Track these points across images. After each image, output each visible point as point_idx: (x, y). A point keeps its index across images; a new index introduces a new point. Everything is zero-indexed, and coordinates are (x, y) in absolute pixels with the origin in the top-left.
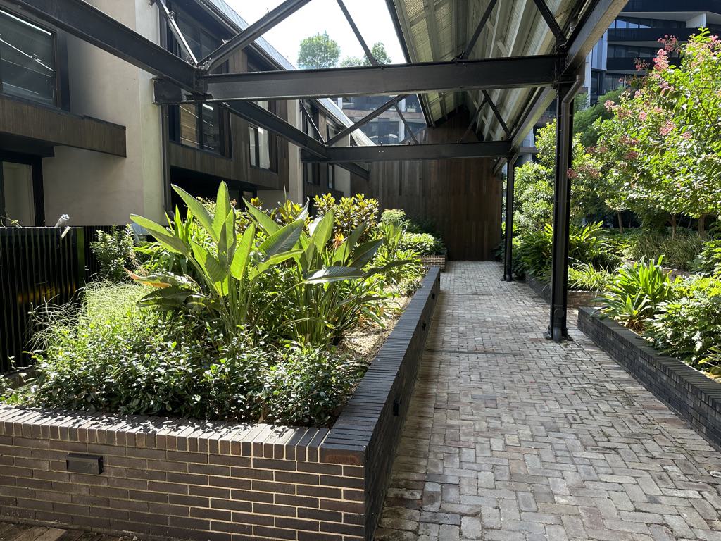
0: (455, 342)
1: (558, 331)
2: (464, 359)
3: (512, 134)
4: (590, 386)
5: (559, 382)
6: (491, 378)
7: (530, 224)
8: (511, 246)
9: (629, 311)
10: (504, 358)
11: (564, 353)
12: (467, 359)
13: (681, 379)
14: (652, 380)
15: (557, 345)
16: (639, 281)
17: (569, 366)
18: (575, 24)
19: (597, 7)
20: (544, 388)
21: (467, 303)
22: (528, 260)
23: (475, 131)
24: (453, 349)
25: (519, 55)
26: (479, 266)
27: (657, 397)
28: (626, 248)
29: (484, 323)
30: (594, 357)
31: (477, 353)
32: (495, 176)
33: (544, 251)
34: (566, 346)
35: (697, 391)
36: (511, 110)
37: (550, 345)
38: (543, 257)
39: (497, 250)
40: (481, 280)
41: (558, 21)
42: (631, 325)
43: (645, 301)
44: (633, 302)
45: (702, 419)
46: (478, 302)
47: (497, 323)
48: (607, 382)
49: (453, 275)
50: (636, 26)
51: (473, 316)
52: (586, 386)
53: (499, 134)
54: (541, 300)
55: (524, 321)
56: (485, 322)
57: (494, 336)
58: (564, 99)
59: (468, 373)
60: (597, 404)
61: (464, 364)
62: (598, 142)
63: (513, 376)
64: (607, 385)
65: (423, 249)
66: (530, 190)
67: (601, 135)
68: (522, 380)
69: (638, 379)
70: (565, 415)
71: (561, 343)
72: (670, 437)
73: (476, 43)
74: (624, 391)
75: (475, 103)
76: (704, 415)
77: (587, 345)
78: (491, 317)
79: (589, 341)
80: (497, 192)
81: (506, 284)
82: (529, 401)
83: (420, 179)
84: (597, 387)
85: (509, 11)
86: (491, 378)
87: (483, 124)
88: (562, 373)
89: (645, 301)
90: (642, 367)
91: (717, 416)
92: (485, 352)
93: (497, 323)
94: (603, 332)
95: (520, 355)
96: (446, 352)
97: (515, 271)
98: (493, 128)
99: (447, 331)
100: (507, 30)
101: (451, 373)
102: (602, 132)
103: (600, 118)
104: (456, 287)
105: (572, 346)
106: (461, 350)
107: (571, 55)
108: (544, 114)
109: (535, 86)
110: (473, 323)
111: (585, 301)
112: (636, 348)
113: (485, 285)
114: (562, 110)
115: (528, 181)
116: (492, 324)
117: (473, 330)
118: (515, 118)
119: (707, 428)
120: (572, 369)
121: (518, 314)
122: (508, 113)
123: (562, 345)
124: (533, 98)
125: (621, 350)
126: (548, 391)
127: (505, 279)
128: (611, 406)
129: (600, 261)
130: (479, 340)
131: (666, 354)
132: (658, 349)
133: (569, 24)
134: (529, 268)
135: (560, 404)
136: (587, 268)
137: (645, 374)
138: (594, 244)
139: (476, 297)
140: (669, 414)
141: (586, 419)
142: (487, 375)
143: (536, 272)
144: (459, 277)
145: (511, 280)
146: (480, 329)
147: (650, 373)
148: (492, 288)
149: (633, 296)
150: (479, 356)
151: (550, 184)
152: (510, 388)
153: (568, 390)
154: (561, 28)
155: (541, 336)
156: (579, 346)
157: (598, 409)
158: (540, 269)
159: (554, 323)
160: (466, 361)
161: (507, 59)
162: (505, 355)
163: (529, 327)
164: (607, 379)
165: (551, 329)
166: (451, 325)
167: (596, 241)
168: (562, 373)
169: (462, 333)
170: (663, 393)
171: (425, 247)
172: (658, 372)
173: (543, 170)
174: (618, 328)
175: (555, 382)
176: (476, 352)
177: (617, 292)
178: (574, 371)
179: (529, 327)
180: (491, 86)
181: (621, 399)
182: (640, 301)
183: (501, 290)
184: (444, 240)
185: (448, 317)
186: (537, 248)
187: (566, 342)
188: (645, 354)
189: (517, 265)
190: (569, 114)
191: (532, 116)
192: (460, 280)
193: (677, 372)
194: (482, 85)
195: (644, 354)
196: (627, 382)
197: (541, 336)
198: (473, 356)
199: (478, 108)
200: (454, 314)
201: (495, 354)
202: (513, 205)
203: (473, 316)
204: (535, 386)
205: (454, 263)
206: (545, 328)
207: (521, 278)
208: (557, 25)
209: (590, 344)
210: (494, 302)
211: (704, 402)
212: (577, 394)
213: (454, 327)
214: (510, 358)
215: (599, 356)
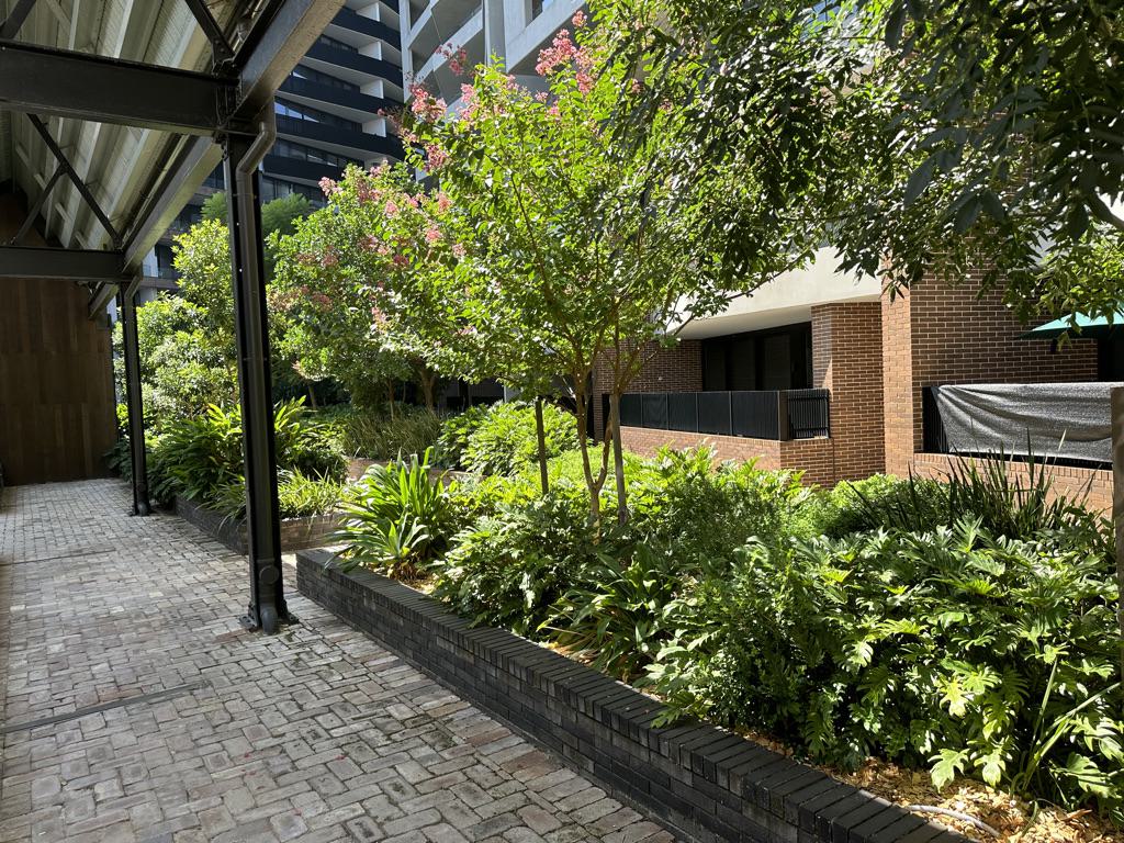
0: (41, 692)
1: (269, 610)
2: (69, 739)
3: (125, 240)
4: (365, 723)
5: (304, 732)
6: (148, 777)
7: (173, 405)
8: (144, 449)
9: (392, 550)
10: (170, 705)
11: (289, 655)
12: (78, 736)
13: (531, 673)
14: (469, 679)
15: (271, 639)
16: (400, 494)
17: (310, 684)
18: (246, 28)
19: (252, 58)
20: (278, 763)
21: (61, 580)
22: (182, 473)
23: (42, 234)
24: (37, 716)
25: (138, 59)
26: (78, 489)
27: (483, 711)
28: (331, 437)
29: (107, 624)
30: (348, 649)
31: (101, 710)
32: (93, 319)
33: (211, 454)
34: (289, 638)
35: (566, 694)
36: (120, 191)
37: (260, 643)
38: (211, 464)
39: (111, 456)
40: (87, 520)
41: (114, 224)
42: (397, 575)
43: (415, 529)
44: (398, 531)
45: (583, 746)
46: (87, 571)
47: (138, 616)
48: (389, 701)
49: (19, 517)
50: (299, 116)
51: (79, 608)
52: (356, 726)
53: (97, 238)
54: (215, 545)
55: (194, 598)
56: (112, 618)
57: (136, 652)
58: (240, 165)
59: (87, 781)
60: (393, 767)
61: (74, 754)
62: (276, 270)
63: (201, 752)
64: (391, 709)
66: (168, 346)
67: (278, 259)
68: (224, 754)
69: (439, 678)
70: (344, 825)
71: (279, 632)
72: (545, 805)
73: (32, 12)
74: (425, 715)
75: (38, 177)
76: (589, 739)
77: (326, 624)
78: (121, 604)
79: (328, 616)
80: (101, 350)
81: (141, 521)
82: (255, 815)
84: (379, 721)
85: (96, 25)
86: (148, 777)
87: (59, 220)
88: (300, 707)
89: (415, 529)
90: (446, 655)
91: (615, 740)
92: (121, 702)
93: (136, 616)
94: (354, 596)
95: (207, 684)
96: (17, 729)
97: (156, 493)
98: (82, 228)
99: (15, 666)
100: (103, 21)
101: (37, 797)
102: (280, 254)
103: (277, 231)
104: (30, 544)
105: (302, 635)
106: (59, 711)
107: (247, 84)
108: (171, 226)
109: (178, 129)
110: (81, 627)
111: (296, 535)
112: (429, 621)
113: (98, 530)
114: (238, 184)
115: (159, 332)
116: (125, 622)
117: (83, 648)
118: (129, 211)
119: (596, 762)
120: (317, 690)
121: (180, 585)
122: (112, 202)
123: (281, 636)
124: (163, 174)
125: (396, 627)
126: (288, 767)
127: (136, 512)
128: (419, 761)
129: (309, 463)
130: (103, 669)
131: (484, 623)
132: (464, 616)
133: (235, 25)
134: (182, 488)
135: (324, 798)
136: (291, 476)
137: (452, 668)
138: (298, 435)
139: (80, 560)
140: (517, 746)
141: (388, 819)
142: (136, 772)
143: (200, 494)
145: (149, 512)
146: (100, 640)
147: (463, 665)
148: (112, 535)
149: (397, 522)
150: (110, 715)
151: (206, 333)
152: (203, 791)
153: (327, 751)
154: (222, 27)
155: (236, 627)
156: (314, 632)
157: (400, 781)
158: (207, 488)
159: (261, 596)
160: (74, 744)
161: (110, 62)
162: (169, 695)
163: (208, 611)
164: (387, 695)
165: (256, 608)
166: (26, 644)
167: (299, 430)
168: (300, 707)
169: (57, 663)
170: (494, 702)
172: (482, 664)
173: (192, 310)
174: (380, 583)
175: (295, 736)
176: (99, 708)
177: (365, 519)
178: (324, 695)
179: (208, 611)
180: (79, 112)
181: (428, 738)
182: (408, 529)
183: (133, 536)
185: (16, 626)
186: (196, 450)
187: (286, 630)
188: (448, 631)
189: (160, 482)
190: (252, 195)
191: (167, 202)
192: (38, 526)
193: (519, 659)
194: (56, 105)
195: (446, 632)
196: (423, 690)
197: (236, 627)
198: (92, 722)
199: (44, 186)
200: (32, 615)
201: (148, 699)
202: (138, 372)
203: (79, 608)
204: (257, 765)
205: (20, 488)
206: (241, 602)
207: (168, 506)
208: (213, 20)
209: (331, 622)
210: (123, 566)
211: (585, 714)
212: (346, 754)
213: (34, 648)
214: (183, 701)
215: (356, 644)
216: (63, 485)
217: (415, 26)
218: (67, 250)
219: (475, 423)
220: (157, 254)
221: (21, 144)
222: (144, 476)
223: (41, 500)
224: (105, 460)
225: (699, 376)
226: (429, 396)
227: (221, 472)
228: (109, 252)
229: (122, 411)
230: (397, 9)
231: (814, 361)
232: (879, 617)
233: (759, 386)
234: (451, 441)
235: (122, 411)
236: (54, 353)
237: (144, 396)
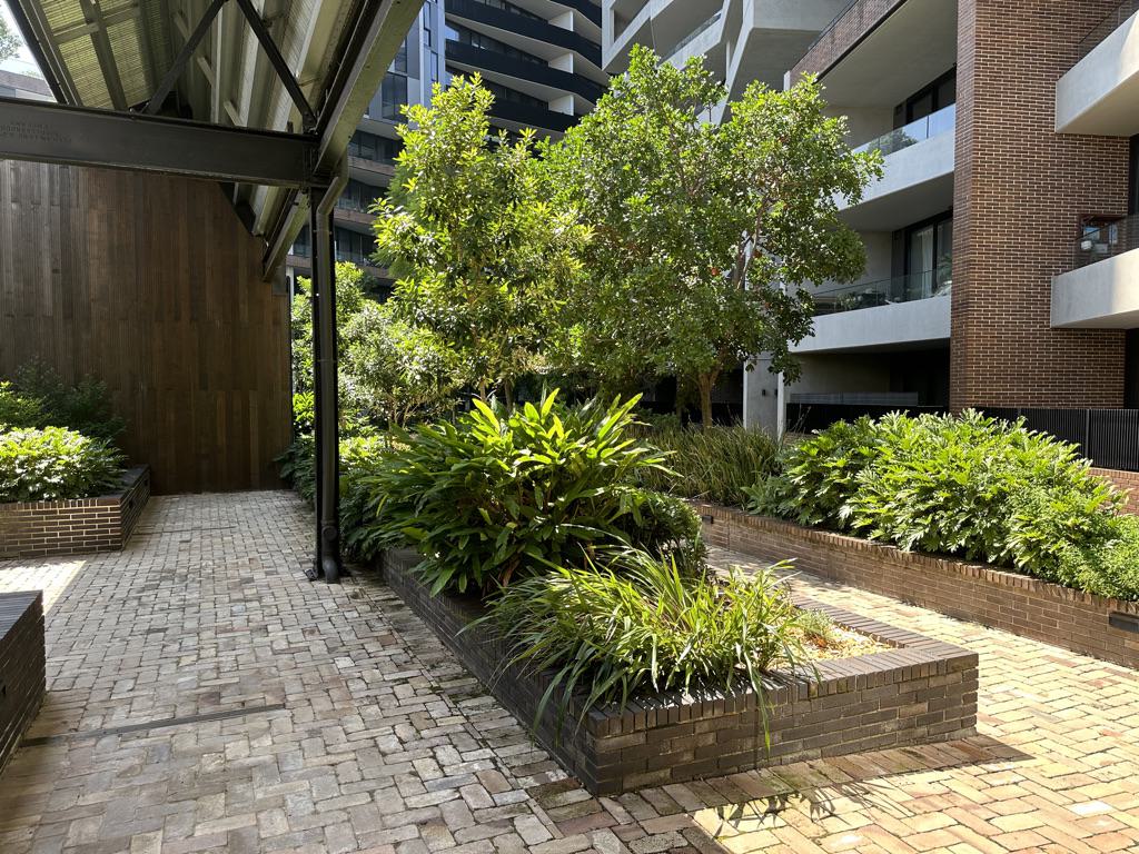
32: (268, 281)
39: (283, 462)
65: (40, 480)
81: (321, 585)
83: (55, 271)
98: (264, 104)
127: (318, 574)
144: (169, 575)
145: (339, 576)
171: (47, 472)
180: (257, 178)
184: (120, 442)
217: (620, 39)
218: (216, 127)
221: (181, 13)
222: (335, 515)
223: (187, 525)
224: (275, 467)
227: (502, 540)
228: (297, 137)
229: (303, 403)
230: (599, 23)
235: (303, 403)
236: (218, 323)
237: (340, 384)
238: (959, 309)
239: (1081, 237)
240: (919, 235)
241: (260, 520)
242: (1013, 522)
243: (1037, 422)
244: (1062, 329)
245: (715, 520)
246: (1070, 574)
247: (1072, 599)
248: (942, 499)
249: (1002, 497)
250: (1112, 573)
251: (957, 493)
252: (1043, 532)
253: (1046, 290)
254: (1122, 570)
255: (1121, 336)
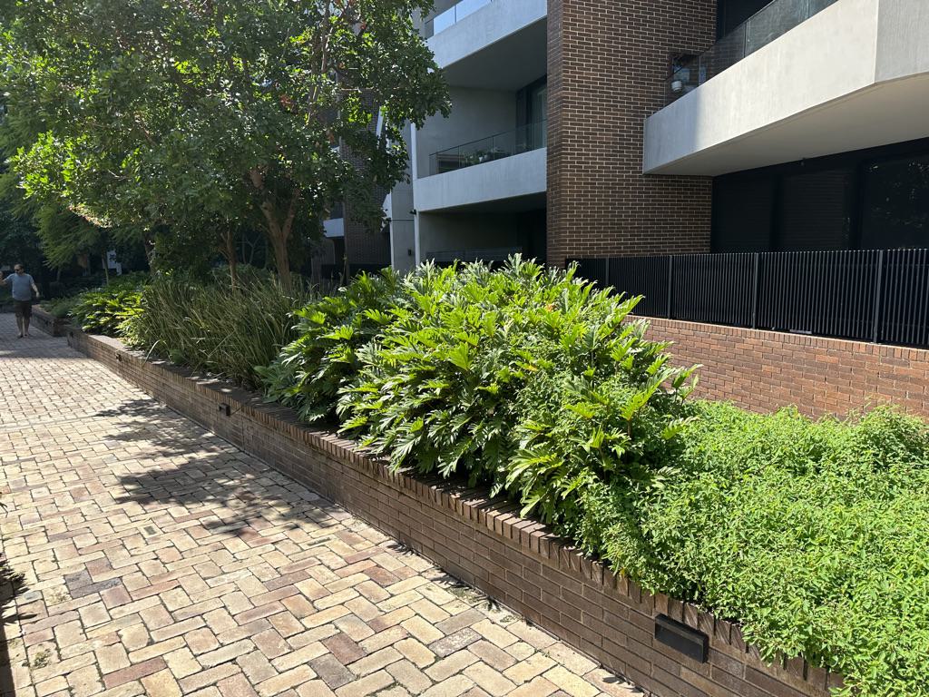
216: (551, 232)
219: (373, 315)
220: (11, 290)
225: (707, 234)
226: (281, 253)
231: (548, 252)
232: (609, 675)
233: (855, 243)
234: (316, 354)
238: (552, 158)
239: (670, 78)
240: (539, 94)
241: (38, 391)
242: (525, 429)
243: (595, 271)
244: (654, 176)
245: (232, 411)
246: (595, 534)
247: (599, 581)
248: (438, 391)
249: (510, 389)
250: (660, 544)
251: (458, 380)
252: (560, 453)
253: (639, 133)
254: (675, 540)
255: (708, 183)
